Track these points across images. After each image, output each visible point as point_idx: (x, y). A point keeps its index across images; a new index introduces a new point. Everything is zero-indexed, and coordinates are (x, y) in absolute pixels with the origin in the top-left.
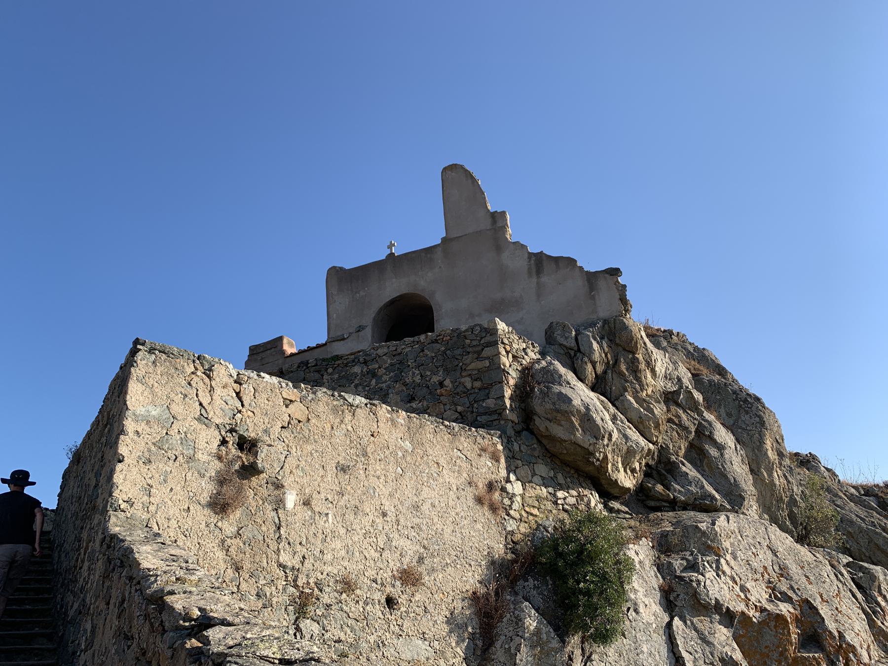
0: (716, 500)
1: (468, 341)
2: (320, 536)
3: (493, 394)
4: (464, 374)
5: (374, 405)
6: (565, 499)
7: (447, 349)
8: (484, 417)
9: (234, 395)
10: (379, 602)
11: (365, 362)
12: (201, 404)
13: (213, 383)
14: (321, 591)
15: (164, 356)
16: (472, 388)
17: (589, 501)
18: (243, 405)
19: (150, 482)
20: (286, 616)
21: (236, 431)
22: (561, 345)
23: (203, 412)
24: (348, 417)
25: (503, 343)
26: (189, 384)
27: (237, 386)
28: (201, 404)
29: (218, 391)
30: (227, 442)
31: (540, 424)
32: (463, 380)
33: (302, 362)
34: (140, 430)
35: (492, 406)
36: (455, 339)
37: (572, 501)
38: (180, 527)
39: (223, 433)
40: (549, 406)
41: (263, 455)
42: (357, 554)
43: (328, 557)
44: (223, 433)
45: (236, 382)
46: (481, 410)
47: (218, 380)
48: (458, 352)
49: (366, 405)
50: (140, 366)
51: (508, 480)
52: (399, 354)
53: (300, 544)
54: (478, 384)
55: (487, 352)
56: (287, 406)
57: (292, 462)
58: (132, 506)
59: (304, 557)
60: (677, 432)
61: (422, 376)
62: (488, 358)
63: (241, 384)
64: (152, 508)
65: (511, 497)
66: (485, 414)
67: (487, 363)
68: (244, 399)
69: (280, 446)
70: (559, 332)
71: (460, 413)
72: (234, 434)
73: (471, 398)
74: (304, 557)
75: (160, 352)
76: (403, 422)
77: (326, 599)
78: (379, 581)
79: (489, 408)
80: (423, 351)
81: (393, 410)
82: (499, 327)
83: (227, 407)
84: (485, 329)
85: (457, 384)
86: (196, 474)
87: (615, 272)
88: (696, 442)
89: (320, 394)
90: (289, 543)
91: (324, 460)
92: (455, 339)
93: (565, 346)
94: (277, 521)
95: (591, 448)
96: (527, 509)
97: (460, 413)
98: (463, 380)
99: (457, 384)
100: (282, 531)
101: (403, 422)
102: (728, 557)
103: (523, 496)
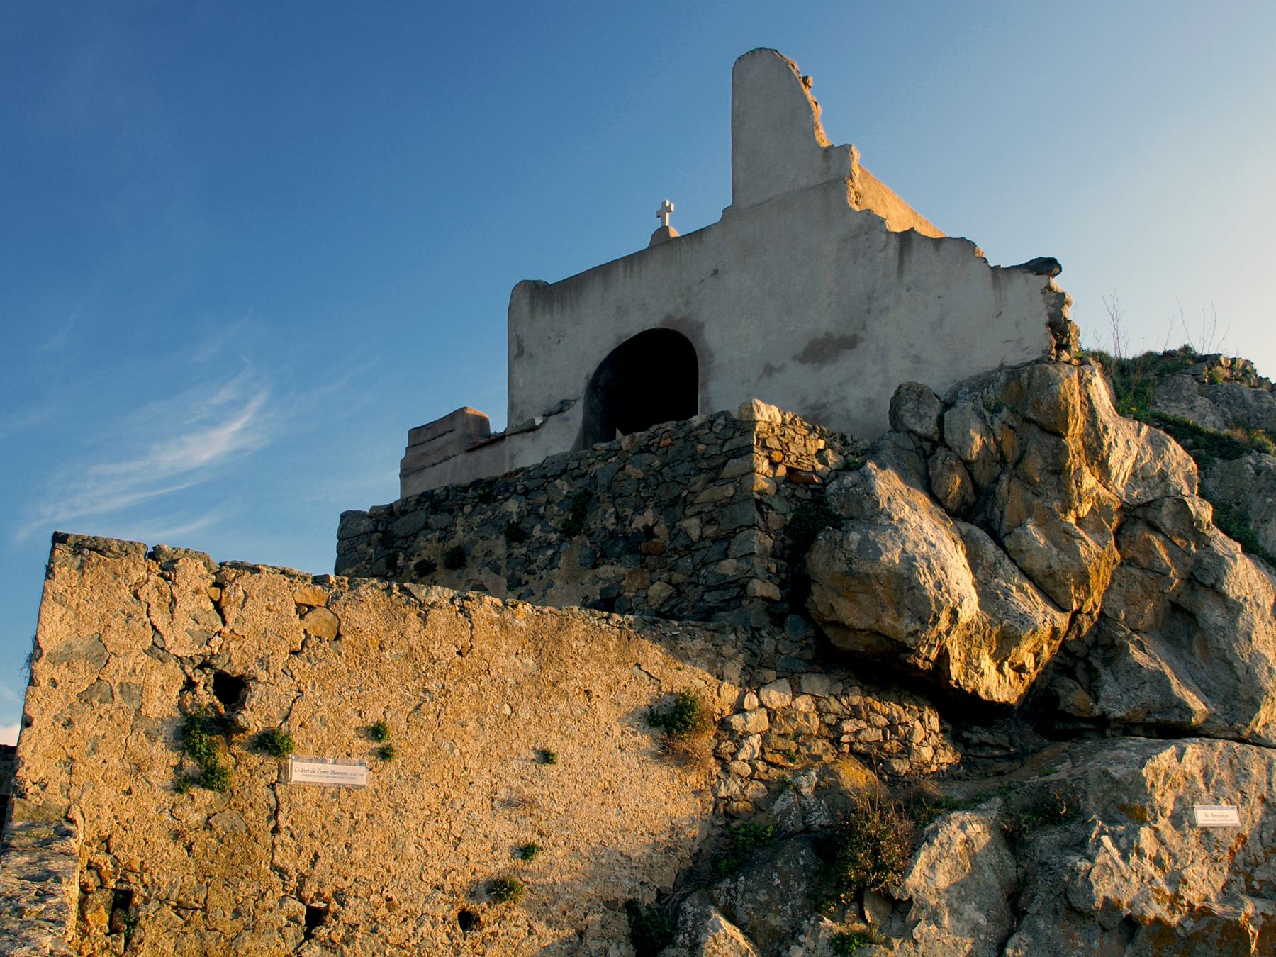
0: (1190, 712)
1: (701, 447)
2: (347, 823)
3: (735, 549)
4: (688, 512)
5: (468, 598)
6: (857, 733)
7: (664, 465)
8: (716, 594)
9: (211, 606)
10: (444, 919)
11: (526, 492)
12: (154, 628)
13: (175, 590)
14: (342, 904)
15: (95, 557)
16: (702, 538)
17: (911, 732)
18: (224, 623)
19: (70, 752)
20: (280, 941)
21: (210, 666)
22: (911, 431)
23: (157, 639)
24: (415, 624)
25: (765, 447)
26: (136, 596)
27: (215, 593)
28: (154, 628)
29: (182, 605)
30: (194, 684)
31: (820, 598)
32: (685, 524)
33: (423, 494)
34: (56, 677)
35: (731, 573)
36: (679, 443)
37: (872, 735)
38: (116, 817)
39: (189, 670)
40: (840, 567)
41: (254, 701)
42: (412, 848)
43: (360, 855)
44: (189, 670)
45: (215, 584)
46: (712, 581)
47: (183, 584)
48: (682, 469)
49: (452, 599)
50: (59, 577)
51: (739, 709)
52: (583, 475)
53: (311, 835)
54: (710, 531)
55: (734, 467)
56: (302, 617)
57: (303, 707)
58: (44, 788)
59: (316, 856)
60: (1142, 583)
61: (617, 518)
62: (733, 479)
63: (222, 587)
64: (75, 792)
65: (739, 739)
66: (717, 588)
67: (730, 491)
68: (227, 610)
69: (286, 682)
70: (910, 405)
71: (676, 586)
72: (208, 670)
73: (697, 559)
74: (316, 856)
75: (90, 549)
76: (523, 624)
77: (349, 915)
78: (448, 887)
79: (725, 576)
80: (623, 468)
81: (506, 605)
82: (758, 417)
83: (197, 628)
84: (734, 422)
85: (675, 531)
86: (143, 738)
87: (1047, 266)
88: (1183, 600)
89: (362, 590)
90: (292, 835)
91: (362, 702)
92: (679, 443)
93: (915, 433)
94: (272, 801)
95: (911, 641)
96: (769, 757)
97: (676, 586)
98: (685, 524)
99: (675, 531)
100: (281, 817)
101: (523, 624)
102: (1163, 823)
103: (765, 737)
